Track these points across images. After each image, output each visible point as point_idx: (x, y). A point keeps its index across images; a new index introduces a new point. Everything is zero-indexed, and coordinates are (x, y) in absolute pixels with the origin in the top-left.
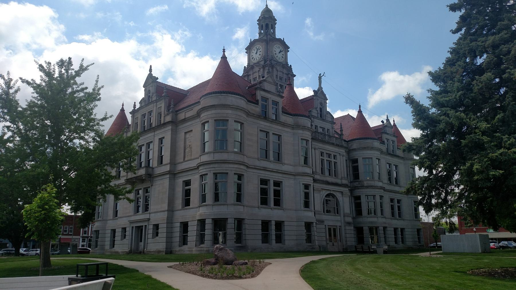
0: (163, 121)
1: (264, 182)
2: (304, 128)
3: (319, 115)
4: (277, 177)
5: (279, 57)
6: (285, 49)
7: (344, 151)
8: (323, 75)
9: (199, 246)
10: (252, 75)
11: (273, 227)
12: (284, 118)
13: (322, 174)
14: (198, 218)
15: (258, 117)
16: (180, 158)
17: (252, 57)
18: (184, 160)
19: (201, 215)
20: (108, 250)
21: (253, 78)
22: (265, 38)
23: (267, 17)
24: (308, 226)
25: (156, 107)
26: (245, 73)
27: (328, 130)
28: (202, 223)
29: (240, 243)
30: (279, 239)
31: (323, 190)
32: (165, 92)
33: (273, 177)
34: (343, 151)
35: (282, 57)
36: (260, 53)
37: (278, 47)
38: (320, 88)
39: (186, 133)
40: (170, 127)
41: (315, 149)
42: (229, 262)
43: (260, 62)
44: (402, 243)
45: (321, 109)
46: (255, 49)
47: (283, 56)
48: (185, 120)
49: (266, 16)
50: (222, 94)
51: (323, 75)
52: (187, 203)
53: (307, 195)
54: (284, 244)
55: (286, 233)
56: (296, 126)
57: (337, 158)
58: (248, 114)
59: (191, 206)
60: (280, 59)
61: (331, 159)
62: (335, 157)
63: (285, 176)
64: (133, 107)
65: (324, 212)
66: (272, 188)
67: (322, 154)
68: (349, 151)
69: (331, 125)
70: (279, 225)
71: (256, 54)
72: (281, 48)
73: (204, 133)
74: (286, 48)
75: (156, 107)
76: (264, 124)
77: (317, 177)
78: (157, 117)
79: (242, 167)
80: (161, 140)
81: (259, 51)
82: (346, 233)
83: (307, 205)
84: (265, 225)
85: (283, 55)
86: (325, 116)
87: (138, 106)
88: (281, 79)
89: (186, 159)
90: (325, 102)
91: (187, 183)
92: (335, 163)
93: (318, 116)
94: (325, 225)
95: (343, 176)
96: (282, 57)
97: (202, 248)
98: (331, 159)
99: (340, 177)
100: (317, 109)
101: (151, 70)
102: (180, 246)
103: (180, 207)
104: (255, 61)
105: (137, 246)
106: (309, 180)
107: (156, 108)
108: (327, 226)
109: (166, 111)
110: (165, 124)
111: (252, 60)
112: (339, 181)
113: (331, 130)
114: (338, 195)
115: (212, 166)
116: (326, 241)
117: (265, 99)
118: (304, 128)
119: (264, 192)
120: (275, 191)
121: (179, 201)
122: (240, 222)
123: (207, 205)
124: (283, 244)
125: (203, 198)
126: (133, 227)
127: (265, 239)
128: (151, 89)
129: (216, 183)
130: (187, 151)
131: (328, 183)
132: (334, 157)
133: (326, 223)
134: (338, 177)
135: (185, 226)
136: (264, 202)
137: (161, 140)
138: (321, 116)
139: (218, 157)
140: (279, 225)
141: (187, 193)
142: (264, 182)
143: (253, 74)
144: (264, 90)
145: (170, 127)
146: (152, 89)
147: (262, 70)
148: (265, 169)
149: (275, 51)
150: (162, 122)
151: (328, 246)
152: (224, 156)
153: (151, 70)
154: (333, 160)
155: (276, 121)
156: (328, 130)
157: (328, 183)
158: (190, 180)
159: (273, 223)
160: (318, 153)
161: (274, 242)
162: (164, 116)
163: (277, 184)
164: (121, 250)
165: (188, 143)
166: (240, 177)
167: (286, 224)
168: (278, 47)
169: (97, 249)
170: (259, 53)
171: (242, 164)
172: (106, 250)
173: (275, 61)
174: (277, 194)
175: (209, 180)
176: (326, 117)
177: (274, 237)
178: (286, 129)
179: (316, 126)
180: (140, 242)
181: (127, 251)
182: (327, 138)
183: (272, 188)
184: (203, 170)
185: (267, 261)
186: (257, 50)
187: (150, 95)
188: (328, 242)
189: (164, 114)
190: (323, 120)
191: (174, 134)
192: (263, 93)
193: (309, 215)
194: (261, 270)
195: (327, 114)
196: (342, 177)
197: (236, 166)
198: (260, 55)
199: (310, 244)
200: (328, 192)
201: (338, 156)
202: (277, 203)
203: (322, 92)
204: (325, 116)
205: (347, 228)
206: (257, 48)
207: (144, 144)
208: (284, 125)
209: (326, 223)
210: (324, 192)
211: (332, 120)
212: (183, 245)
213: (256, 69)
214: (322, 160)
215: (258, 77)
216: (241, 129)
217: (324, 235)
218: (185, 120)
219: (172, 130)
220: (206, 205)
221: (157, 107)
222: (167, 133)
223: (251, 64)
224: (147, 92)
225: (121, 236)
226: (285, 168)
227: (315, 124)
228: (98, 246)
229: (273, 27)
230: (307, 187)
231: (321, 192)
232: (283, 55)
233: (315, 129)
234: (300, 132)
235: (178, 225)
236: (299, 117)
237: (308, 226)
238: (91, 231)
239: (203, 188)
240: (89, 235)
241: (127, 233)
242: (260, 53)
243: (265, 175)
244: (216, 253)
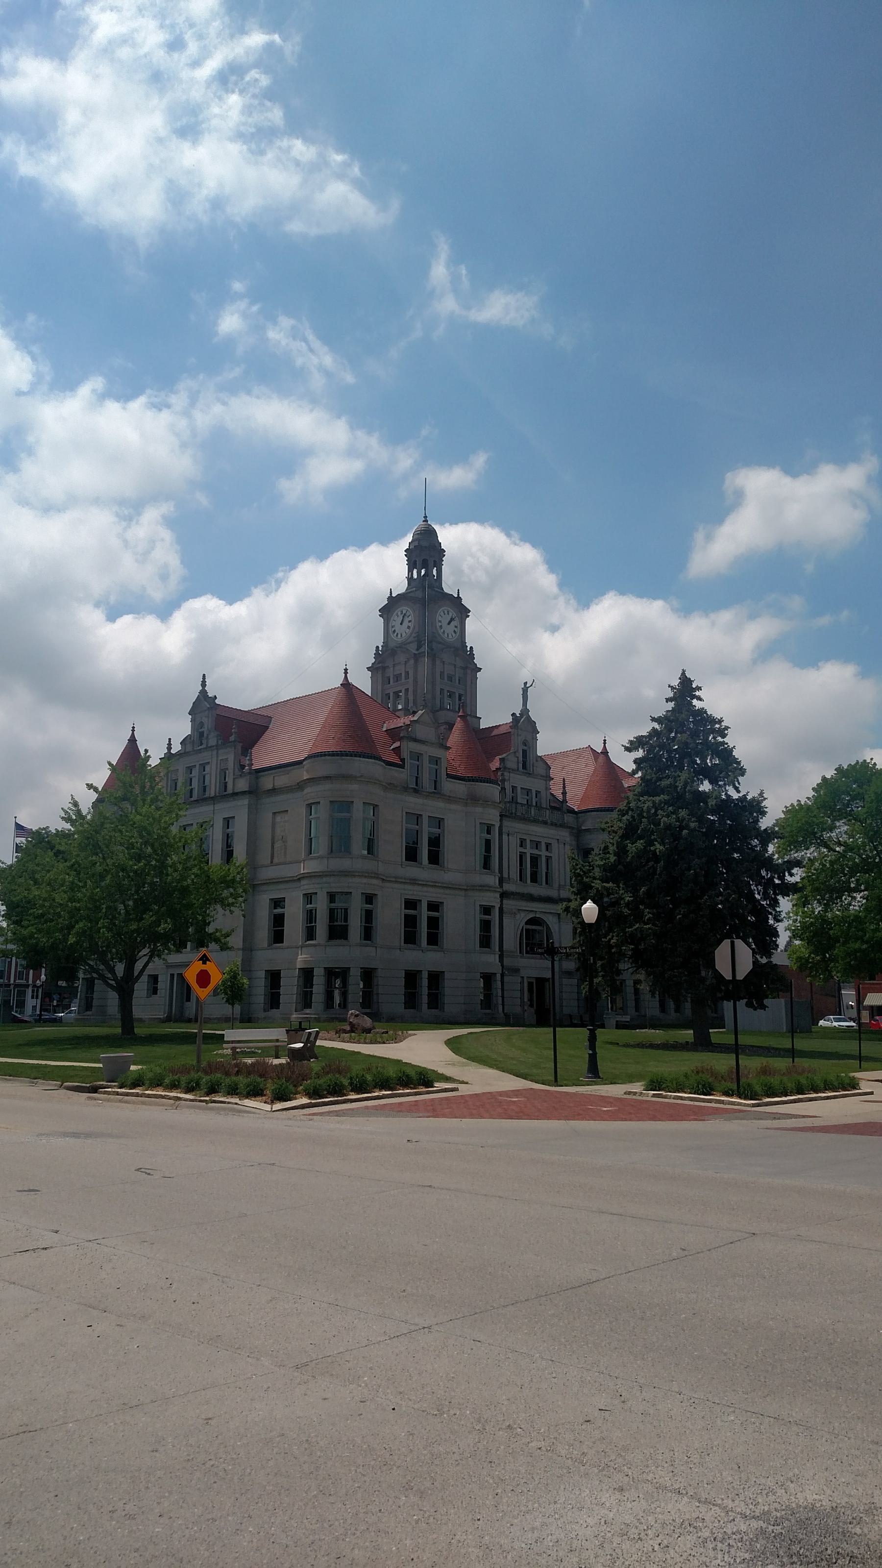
0: (232, 787)
1: (411, 904)
2: (486, 802)
3: (521, 765)
4: (434, 895)
5: (448, 632)
6: (461, 614)
7: (567, 834)
8: (531, 686)
9: (303, 1012)
10: (392, 669)
11: (425, 982)
12: (448, 786)
13: (521, 880)
14: (299, 965)
15: (405, 789)
16: (264, 857)
17: (393, 629)
18: (272, 862)
19: (305, 962)
20: (116, 1015)
21: (394, 676)
22: (419, 594)
23: (426, 547)
24: (488, 978)
25: (217, 757)
26: (379, 663)
27: (537, 793)
28: (307, 974)
29: (369, 1008)
30: (435, 1001)
31: (520, 911)
32: (235, 733)
33: (426, 895)
34: (565, 835)
35: (455, 631)
36: (410, 624)
37: (446, 612)
38: (525, 711)
39: (274, 813)
40: (246, 802)
41: (508, 835)
42: (369, 1031)
43: (409, 643)
44: (676, 1012)
45: (524, 752)
46: (399, 613)
47: (456, 629)
48: (274, 791)
49: (424, 544)
50: (343, 757)
51: (531, 686)
52: (278, 937)
53: (486, 926)
54: (444, 1011)
55: (447, 991)
56: (473, 799)
57: (551, 849)
58: (389, 787)
59: (285, 943)
60: (450, 637)
61: (541, 851)
62: (548, 846)
63: (448, 891)
64: (167, 748)
65: (520, 953)
66: (424, 914)
67: (522, 843)
68: (578, 833)
69: (545, 782)
70: (436, 978)
71: (401, 624)
72: (453, 613)
73: (311, 821)
74: (464, 612)
75: (217, 757)
76: (414, 803)
77: (508, 887)
78: (218, 777)
79: (374, 881)
80: (227, 822)
81: (406, 620)
82: (561, 992)
83: (485, 942)
84: (411, 977)
85: (456, 627)
86: (533, 766)
87: (176, 748)
88: (450, 678)
89: (276, 860)
90: (533, 738)
91: (278, 903)
92: (548, 859)
93: (518, 768)
94: (523, 977)
95: (562, 883)
96: (455, 631)
97: (86, 1015)
98: (541, 851)
99: (556, 885)
100: (517, 753)
101: (204, 684)
102: (265, 1011)
103: (265, 944)
104: (399, 640)
105: (182, 1008)
106: (492, 899)
107: (217, 760)
108: (525, 978)
109: (236, 769)
110: (235, 794)
111: (393, 636)
112: (553, 893)
113: (543, 794)
114: (551, 921)
115: (324, 879)
116: (522, 1004)
117: (418, 756)
118: (486, 802)
119: (411, 922)
120: (430, 919)
121: (263, 933)
122: (368, 975)
123: (316, 946)
124: (440, 1010)
125: (310, 934)
126: (172, 975)
127: (411, 1001)
128: (205, 720)
129: (330, 909)
130: (277, 845)
131: (531, 898)
132: (547, 847)
133: (524, 973)
134: (552, 886)
135: (274, 977)
136: (410, 938)
137: (227, 822)
138: (524, 767)
139: (336, 864)
140: (436, 978)
141: (278, 921)
142: (411, 904)
143: (394, 667)
144: (415, 740)
145: (246, 802)
146: (208, 723)
147: (412, 662)
148: (413, 882)
149: (440, 621)
150: (230, 790)
151: (526, 1014)
152: (345, 864)
153: (204, 684)
154: (543, 853)
155: (436, 791)
156: (537, 793)
157: (531, 898)
158: (284, 898)
159: (425, 975)
160: (514, 841)
161: (425, 1006)
162: (234, 779)
163: (434, 906)
164: (147, 1015)
165: (278, 831)
166: (369, 899)
167: (447, 975)
168: (446, 612)
169: (88, 1013)
170: (406, 623)
171: (376, 876)
172: (110, 1015)
173: (440, 643)
174: (434, 923)
175: (321, 906)
176: (535, 768)
177: (425, 999)
178: (453, 807)
179: (514, 788)
180: (187, 1001)
181: (162, 1017)
182: (533, 813)
183: (424, 914)
184: (308, 886)
185: (410, 1032)
186: (403, 617)
187: (203, 732)
188: (526, 1008)
189: (234, 775)
190: (530, 774)
191: (254, 811)
192: (413, 746)
193: (490, 961)
194: (404, 1039)
195: (537, 761)
196: (560, 885)
197: (365, 880)
198: (409, 627)
199: (488, 1011)
200: (531, 915)
201: (555, 845)
202: (434, 939)
203: (529, 718)
204: (533, 766)
205: (565, 981)
206: (404, 612)
207: (192, 824)
208: (450, 799)
209: (524, 973)
210: (523, 914)
211: (546, 773)
212: (272, 1008)
213: (402, 658)
214: (522, 856)
215: (403, 675)
216: (374, 815)
217: (518, 994)
218: (274, 791)
219: (250, 805)
220: (314, 945)
221: (220, 758)
222: (240, 810)
223: (392, 645)
224: (197, 725)
225: (148, 990)
226: (448, 877)
227: (512, 784)
228: (94, 1009)
229: (439, 564)
230: (487, 910)
231: (518, 916)
232: (456, 627)
233: (513, 793)
234: (479, 810)
235: (262, 974)
236: (477, 783)
237: (488, 978)
238: (16, 972)
239: (311, 916)
240: (12, 981)
241: (160, 985)
242: (410, 624)
243: (412, 892)
244: (351, 1020)
